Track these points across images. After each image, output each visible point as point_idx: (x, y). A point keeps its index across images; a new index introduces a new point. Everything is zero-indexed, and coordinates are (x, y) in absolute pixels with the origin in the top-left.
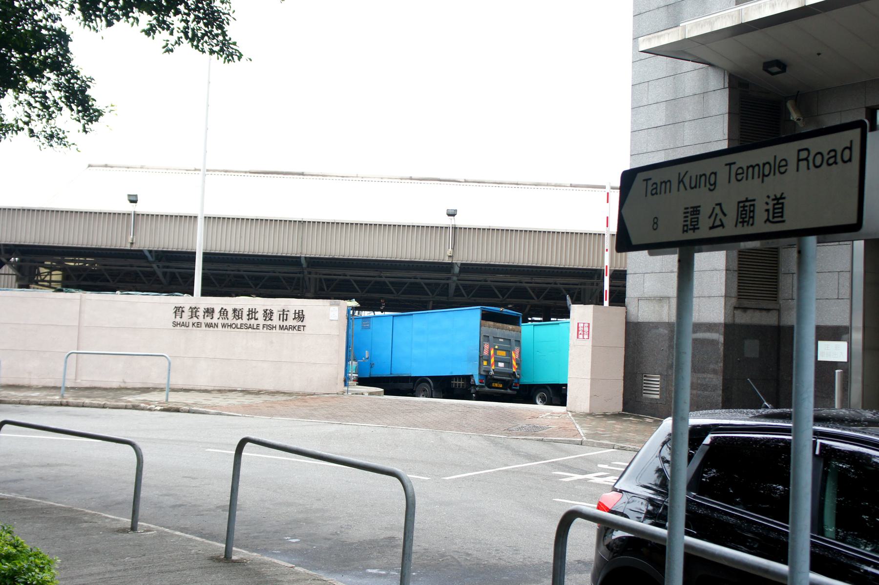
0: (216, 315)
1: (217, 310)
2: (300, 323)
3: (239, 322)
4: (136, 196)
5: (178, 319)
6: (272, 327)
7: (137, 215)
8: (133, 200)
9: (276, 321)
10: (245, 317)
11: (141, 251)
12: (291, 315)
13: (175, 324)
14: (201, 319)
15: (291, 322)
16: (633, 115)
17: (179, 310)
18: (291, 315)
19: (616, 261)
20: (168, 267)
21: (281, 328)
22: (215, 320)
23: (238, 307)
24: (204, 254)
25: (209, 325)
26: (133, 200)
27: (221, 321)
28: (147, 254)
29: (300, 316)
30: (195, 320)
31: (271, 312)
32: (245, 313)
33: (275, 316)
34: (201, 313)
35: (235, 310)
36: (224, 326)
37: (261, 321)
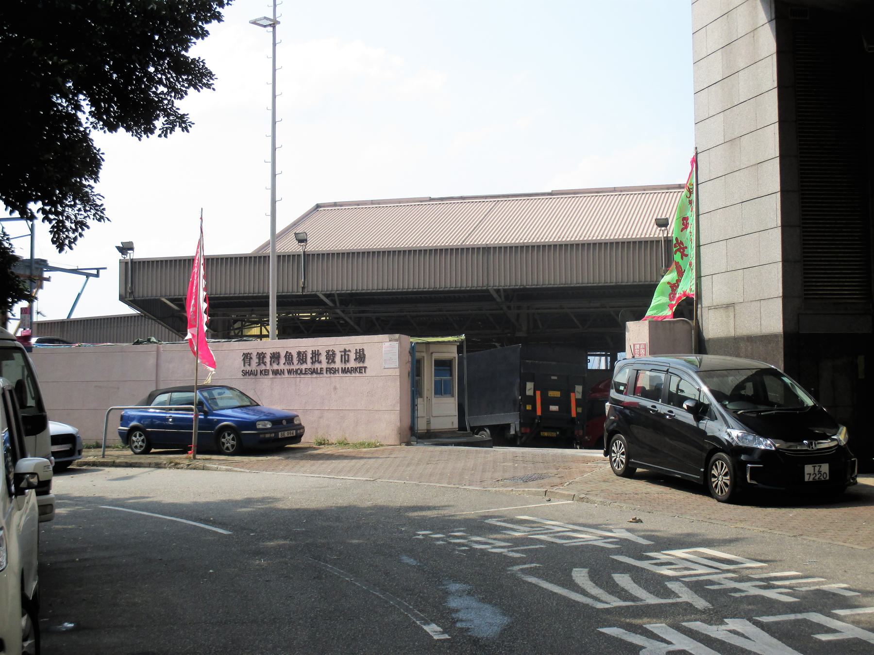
0: (283, 360)
1: (283, 354)
2: (361, 365)
3: (304, 367)
4: (131, 243)
5: (248, 368)
6: (281, 372)
7: (306, 255)
8: (302, 241)
9: (338, 365)
10: (309, 360)
11: (487, 291)
12: (352, 356)
13: (245, 373)
14: (268, 367)
15: (352, 364)
16: (695, 72)
17: (247, 357)
18: (352, 356)
19: (857, 257)
20: (363, 312)
21: (344, 371)
22: (282, 367)
23: (302, 350)
24: (278, 297)
25: (276, 372)
26: (302, 241)
27: (287, 367)
28: (495, 295)
29: (361, 356)
30: (263, 367)
31: (334, 354)
32: (309, 356)
33: (338, 359)
34: (268, 360)
35: (299, 353)
36: (289, 372)
37: (324, 365)
